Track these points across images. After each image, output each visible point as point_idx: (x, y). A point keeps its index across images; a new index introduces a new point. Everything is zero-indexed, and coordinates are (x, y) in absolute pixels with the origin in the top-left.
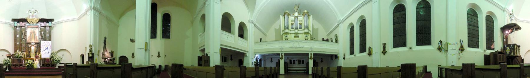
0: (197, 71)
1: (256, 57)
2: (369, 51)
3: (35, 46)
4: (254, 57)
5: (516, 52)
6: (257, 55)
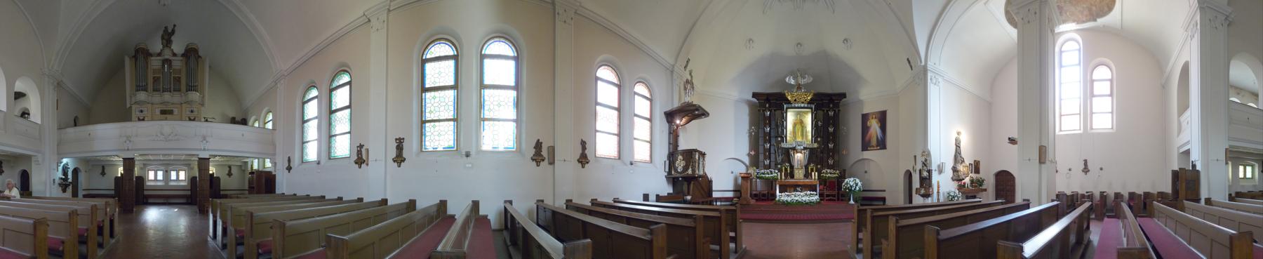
0: (1220, 217)
1: (62, 165)
2: (358, 155)
3: (805, 153)
4: (58, 166)
5: (699, 166)
6: (65, 161)
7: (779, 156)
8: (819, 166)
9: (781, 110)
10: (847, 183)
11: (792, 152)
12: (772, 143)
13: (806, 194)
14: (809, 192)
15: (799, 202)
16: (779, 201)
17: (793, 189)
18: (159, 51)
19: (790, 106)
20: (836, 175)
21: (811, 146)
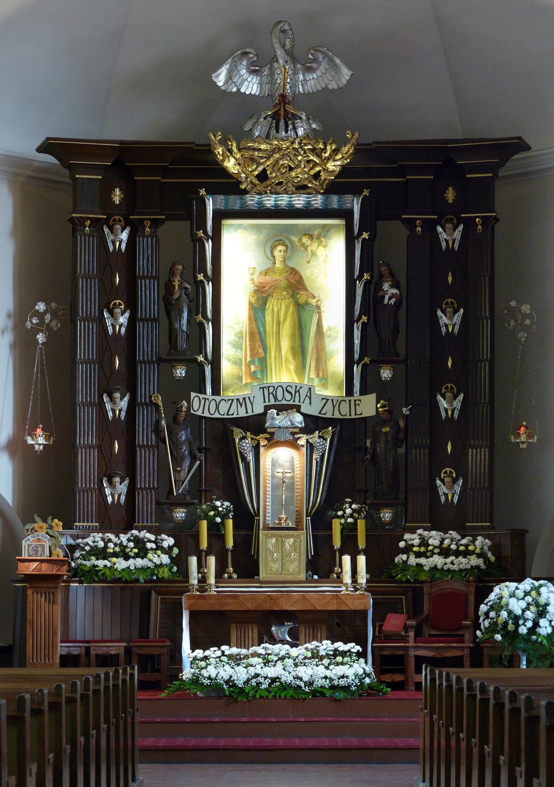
3: (311, 447)
7: (177, 461)
8: (386, 515)
9: (189, 218)
10: (498, 606)
11: (247, 445)
12: (141, 390)
13: (316, 655)
14: (326, 646)
15: (285, 687)
16: (195, 681)
17: (253, 632)
18: (92, 537)
19: (235, 202)
20: (474, 561)
21: (345, 412)
